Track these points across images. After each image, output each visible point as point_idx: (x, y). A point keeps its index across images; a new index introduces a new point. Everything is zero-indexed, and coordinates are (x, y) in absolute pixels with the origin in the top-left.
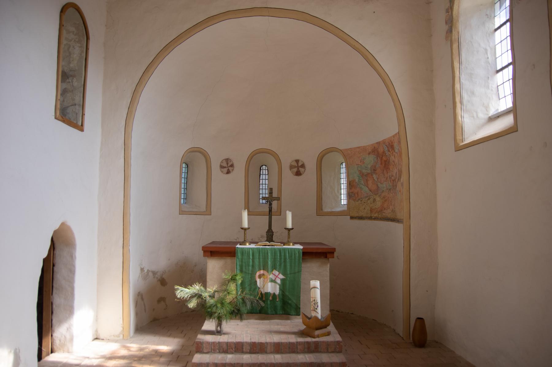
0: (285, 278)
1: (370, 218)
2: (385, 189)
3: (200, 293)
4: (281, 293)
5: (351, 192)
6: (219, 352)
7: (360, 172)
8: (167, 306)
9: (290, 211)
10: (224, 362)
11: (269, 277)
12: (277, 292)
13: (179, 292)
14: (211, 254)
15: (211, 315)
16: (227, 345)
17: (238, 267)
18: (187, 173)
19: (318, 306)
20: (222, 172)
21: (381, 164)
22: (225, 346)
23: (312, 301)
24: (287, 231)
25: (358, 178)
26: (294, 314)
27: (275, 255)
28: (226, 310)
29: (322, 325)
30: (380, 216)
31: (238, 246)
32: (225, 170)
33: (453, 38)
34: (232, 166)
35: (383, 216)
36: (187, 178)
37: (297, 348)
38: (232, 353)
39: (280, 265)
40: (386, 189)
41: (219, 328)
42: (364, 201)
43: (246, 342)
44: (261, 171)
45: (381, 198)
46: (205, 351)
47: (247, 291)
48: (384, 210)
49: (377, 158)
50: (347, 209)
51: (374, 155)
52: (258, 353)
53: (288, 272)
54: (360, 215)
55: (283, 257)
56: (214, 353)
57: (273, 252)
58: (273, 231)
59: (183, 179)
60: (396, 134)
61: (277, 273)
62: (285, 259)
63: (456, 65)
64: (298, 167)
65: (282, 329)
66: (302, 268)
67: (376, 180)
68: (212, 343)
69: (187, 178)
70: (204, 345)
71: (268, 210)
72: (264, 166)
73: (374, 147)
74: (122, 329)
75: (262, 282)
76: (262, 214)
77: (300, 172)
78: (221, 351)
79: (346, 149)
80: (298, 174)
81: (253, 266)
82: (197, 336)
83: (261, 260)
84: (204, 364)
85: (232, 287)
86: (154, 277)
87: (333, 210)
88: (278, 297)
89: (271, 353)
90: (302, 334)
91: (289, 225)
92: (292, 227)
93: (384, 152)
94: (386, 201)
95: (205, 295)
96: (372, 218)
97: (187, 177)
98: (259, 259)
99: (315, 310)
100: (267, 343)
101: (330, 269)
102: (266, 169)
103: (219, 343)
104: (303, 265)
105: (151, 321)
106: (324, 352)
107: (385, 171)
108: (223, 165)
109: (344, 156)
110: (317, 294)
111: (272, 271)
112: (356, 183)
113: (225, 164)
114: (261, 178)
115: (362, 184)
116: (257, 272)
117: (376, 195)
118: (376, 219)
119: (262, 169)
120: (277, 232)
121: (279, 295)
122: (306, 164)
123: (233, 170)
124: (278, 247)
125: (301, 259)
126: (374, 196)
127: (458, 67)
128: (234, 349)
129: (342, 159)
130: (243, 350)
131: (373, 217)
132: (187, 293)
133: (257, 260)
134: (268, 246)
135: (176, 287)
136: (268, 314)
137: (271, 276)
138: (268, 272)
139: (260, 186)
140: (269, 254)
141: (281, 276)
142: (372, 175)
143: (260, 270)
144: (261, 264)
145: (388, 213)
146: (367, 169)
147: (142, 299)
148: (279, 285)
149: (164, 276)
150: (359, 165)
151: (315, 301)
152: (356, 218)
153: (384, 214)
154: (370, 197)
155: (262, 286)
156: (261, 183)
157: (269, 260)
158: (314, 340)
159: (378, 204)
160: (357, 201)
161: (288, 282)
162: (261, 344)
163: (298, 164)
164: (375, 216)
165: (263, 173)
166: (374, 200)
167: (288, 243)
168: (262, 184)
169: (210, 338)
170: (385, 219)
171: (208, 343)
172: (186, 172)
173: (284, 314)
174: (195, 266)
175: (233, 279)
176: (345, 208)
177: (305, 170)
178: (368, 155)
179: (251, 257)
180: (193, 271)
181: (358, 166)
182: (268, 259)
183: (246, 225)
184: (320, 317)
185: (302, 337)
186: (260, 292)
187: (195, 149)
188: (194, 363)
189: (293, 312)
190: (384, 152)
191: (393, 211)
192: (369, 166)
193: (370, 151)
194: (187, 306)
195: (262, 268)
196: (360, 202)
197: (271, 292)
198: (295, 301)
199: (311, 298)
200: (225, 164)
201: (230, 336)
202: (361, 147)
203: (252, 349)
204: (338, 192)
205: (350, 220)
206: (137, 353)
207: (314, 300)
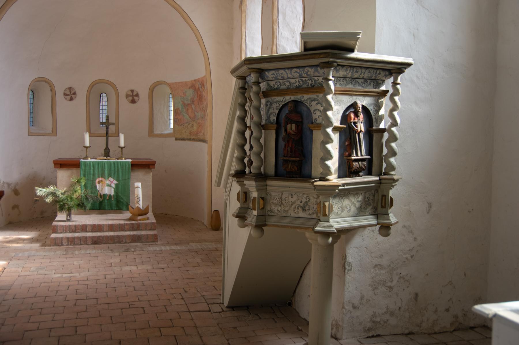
0: (118, 183)
1: (189, 140)
2: (199, 117)
3: (55, 192)
4: (115, 194)
6: (70, 232)
7: (183, 102)
8: (20, 212)
9: (122, 133)
11: (106, 183)
13: (38, 191)
14: (60, 166)
15: (62, 208)
16: (75, 227)
18: (33, 99)
19: (140, 200)
20: (66, 99)
21: (197, 97)
22: (73, 228)
23: (136, 196)
24: (120, 149)
26: (125, 209)
28: (74, 202)
29: (144, 213)
30: (196, 138)
31: (82, 160)
32: (69, 97)
33: (242, 9)
34: (75, 94)
36: (33, 104)
37: (125, 227)
38: (79, 232)
39: (114, 174)
43: (89, 225)
44: (101, 98)
46: (59, 232)
47: (89, 190)
48: (199, 133)
49: (195, 92)
50: (393, 105)
53: (121, 179)
55: (116, 168)
56: (66, 233)
57: (109, 164)
60: (205, 76)
61: (112, 179)
62: (118, 169)
63: (244, 30)
64: (133, 96)
66: (131, 176)
67: (194, 109)
68: (64, 226)
69: (33, 104)
70: (58, 227)
71: (105, 132)
72: (104, 95)
73: (193, 83)
75: (101, 186)
76: (100, 136)
77: (135, 100)
78: (71, 231)
79: (172, 83)
80: (133, 102)
81: (94, 175)
82: (52, 223)
83: (100, 170)
84: (59, 238)
86: (9, 188)
87: (162, 133)
88: (113, 198)
91: (122, 144)
92: (124, 145)
93: (199, 88)
94: (200, 126)
95: (58, 193)
97: (33, 103)
98: (98, 169)
99: (138, 203)
100: (104, 225)
101: (152, 176)
102: (106, 96)
105: (7, 224)
107: (200, 103)
108: (66, 92)
109: (171, 88)
110: (139, 192)
111: (108, 178)
113: (68, 92)
116: (96, 179)
117: (194, 121)
118: (193, 140)
119: (101, 96)
120: (116, 150)
121: (113, 195)
122: (140, 93)
123: (75, 97)
124: (113, 160)
125: (130, 169)
126: (193, 122)
127: (245, 31)
128: (80, 230)
129: (169, 91)
130: (87, 230)
131: (192, 139)
132: (44, 192)
133: (97, 170)
134: (105, 160)
135: (36, 188)
136: (105, 210)
138: (105, 179)
139: (100, 111)
140: (106, 166)
141: (115, 182)
142: (191, 105)
143: (99, 177)
144: (100, 173)
145: (201, 136)
148: (114, 189)
149: (17, 188)
150: (182, 96)
151: (138, 197)
155: (101, 190)
157: (106, 170)
158: (136, 222)
159: (195, 128)
160: (180, 126)
161: (120, 186)
162: (100, 226)
164: (193, 137)
165: (102, 100)
166: (193, 126)
167: (121, 158)
168: (102, 110)
170: (200, 140)
171: (61, 226)
172: (32, 98)
173: (118, 210)
174: (44, 179)
175: (79, 182)
176: (172, 131)
177: (139, 98)
180: (42, 183)
182: (105, 169)
183: (87, 144)
184: (141, 208)
186: (100, 194)
187: (41, 79)
190: (199, 88)
191: (204, 134)
192: (189, 98)
194: (45, 201)
195: (100, 176)
197: (108, 194)
198: (126, 200)
199: (135, 195)
200: (68, 92)
201: (77, 222)
203: (93, 229)
204: (167, 117)
207: (137, 196)
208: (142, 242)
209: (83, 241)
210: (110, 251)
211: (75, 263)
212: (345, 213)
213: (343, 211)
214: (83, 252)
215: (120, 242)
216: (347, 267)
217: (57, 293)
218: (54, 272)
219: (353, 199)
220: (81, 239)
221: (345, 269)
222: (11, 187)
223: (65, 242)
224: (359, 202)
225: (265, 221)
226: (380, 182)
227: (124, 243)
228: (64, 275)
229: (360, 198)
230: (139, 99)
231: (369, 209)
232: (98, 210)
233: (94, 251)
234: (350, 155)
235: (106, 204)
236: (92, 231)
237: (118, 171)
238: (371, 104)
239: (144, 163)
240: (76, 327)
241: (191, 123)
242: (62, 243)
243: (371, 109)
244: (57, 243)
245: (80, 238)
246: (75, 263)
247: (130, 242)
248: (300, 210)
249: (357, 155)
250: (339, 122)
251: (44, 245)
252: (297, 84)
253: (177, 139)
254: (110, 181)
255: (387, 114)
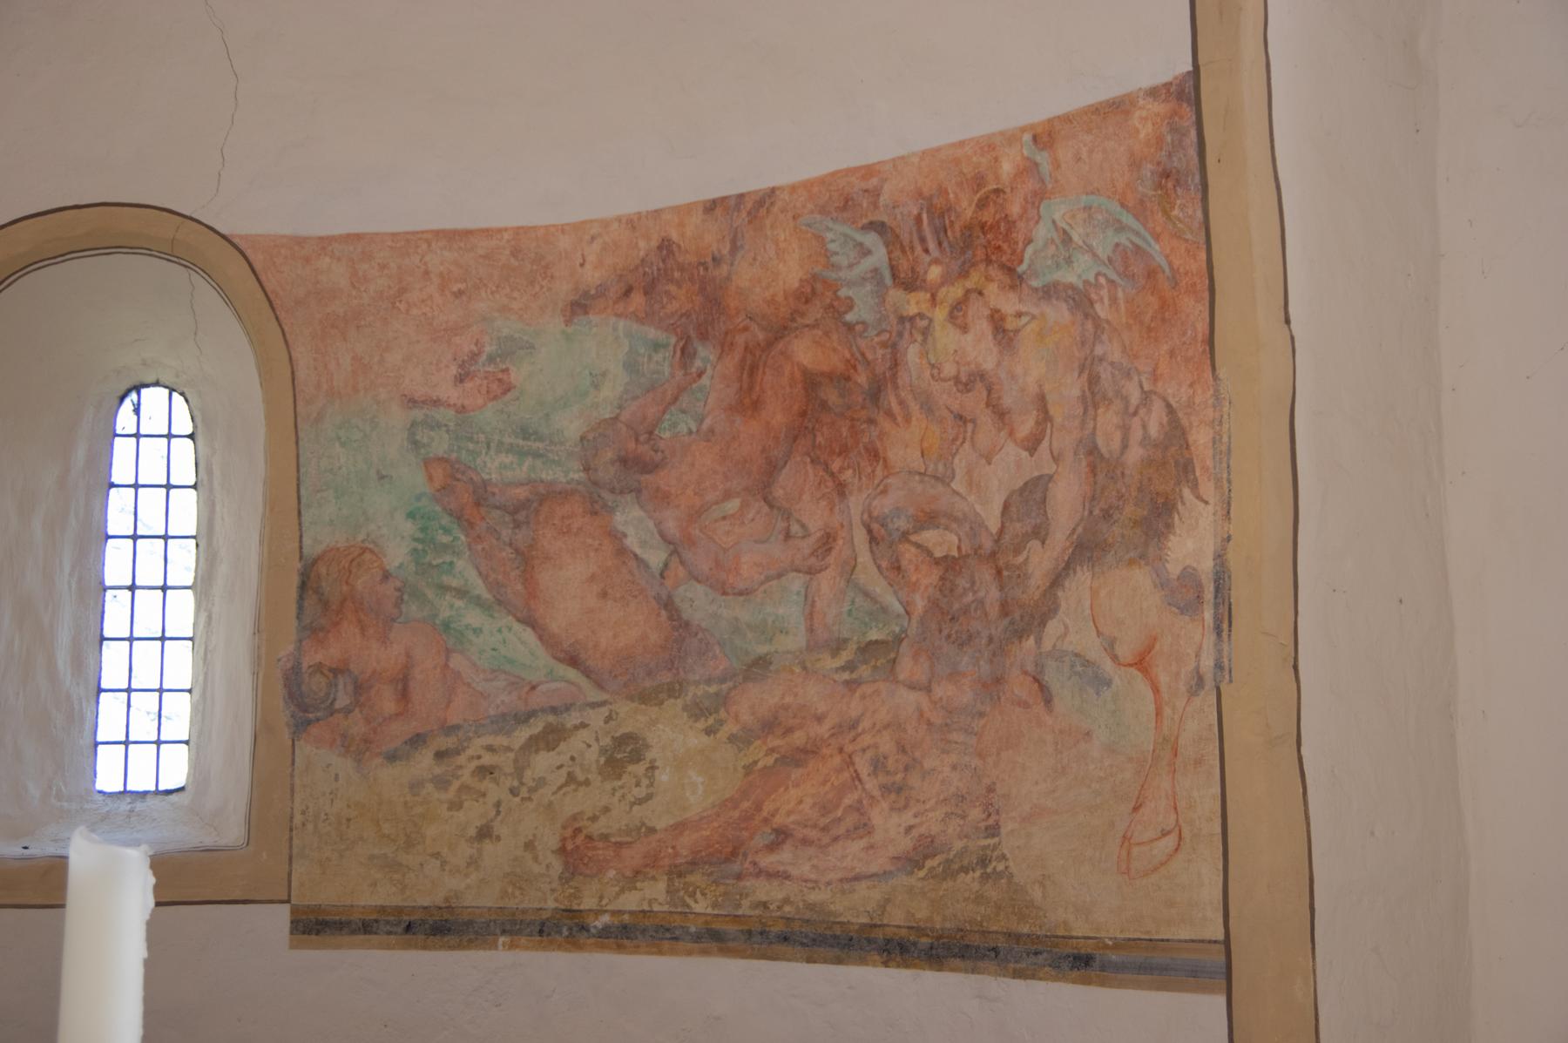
5: (318, 668)
25: (409, 528)
30: (700, 906)
35: (745, 910)
40: (811, 647)
42: (488, 759)
45: (730, 728)
51: (644, 318)
54: (425, 901)
79: (300, 241)
96: (584, 928)
112: (386, 576)
115: (461, 593)
146: (537, 455)
150: (436, 403)
152: (366, 928)
153: (764, 890)
154: (572, 719)
160: (392, 757)
164: (631, 901)
178: (568, 322)
181: (418, 414)
192: (571, 426)
193: (592, 276)
196: (424, 763)
202: (487, 233)
205: (292, 947)
241: (596, 718)
255: (1214, 734)
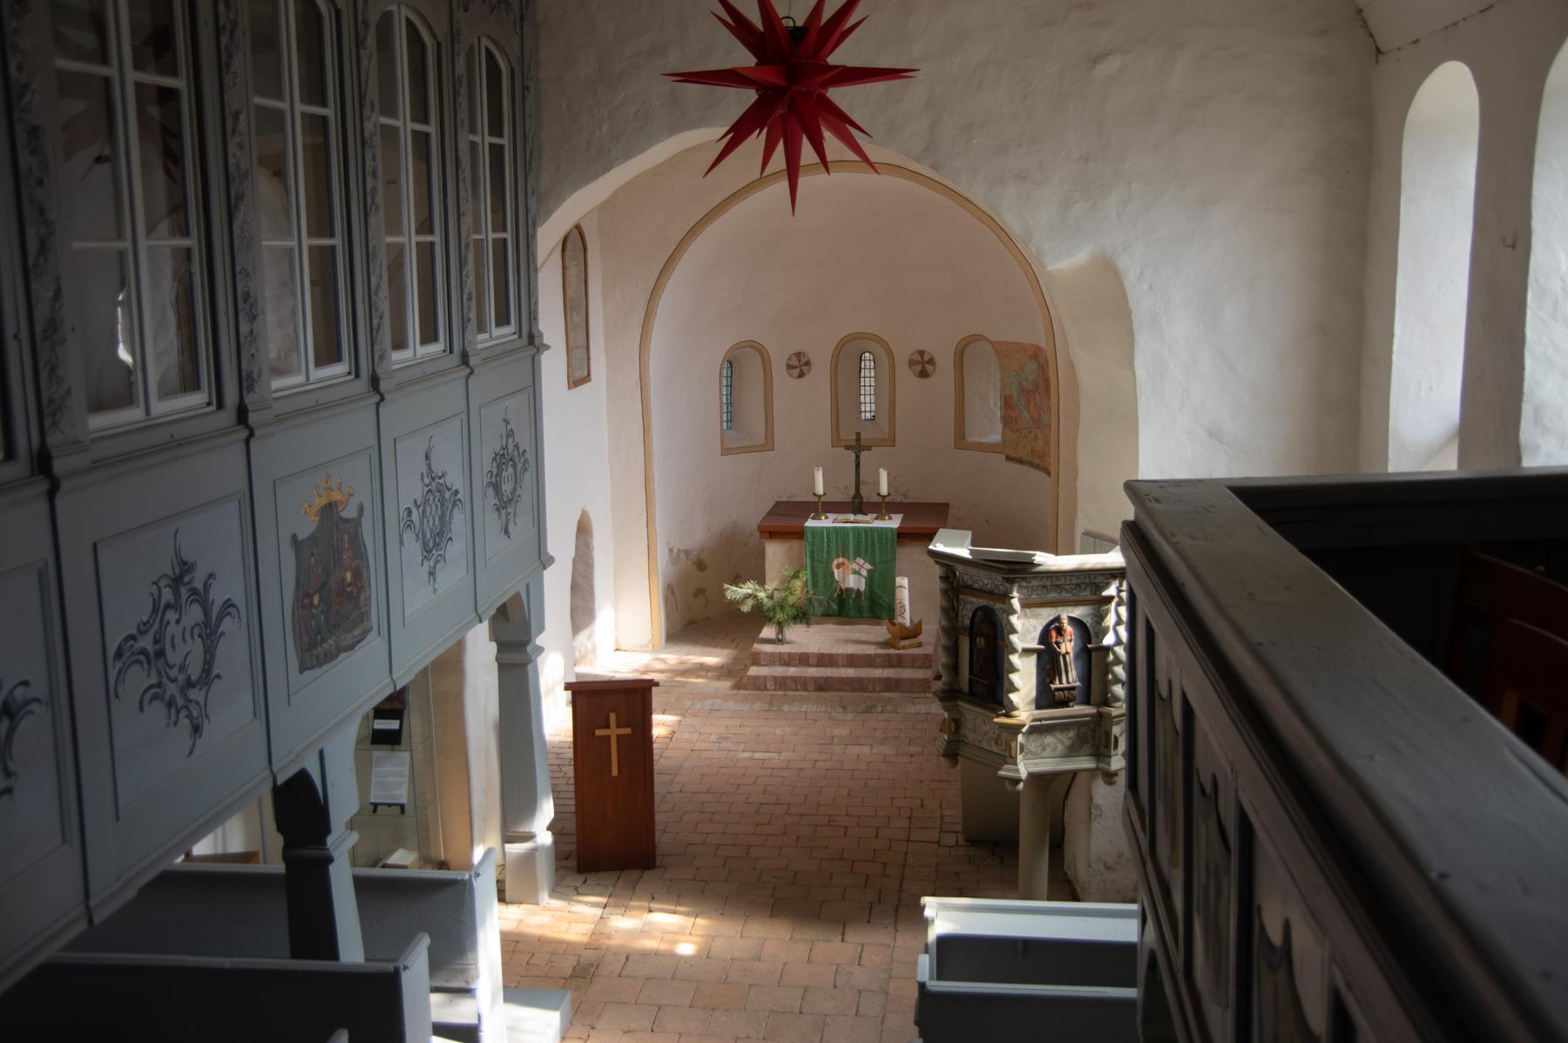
6: (781, 665)
7: (1019, 383)
9: (885, 468)
10: (784, 675)
12: (863, 587)
17: (808, 553)
20: (791, 375)
22: (786, 658)
27: (858, 542)
29: (914, 632)
32: (796, 372)
34: (808, 363)
41: (780, 636)
46: (763, 663)
52: (827, 666)
53: (878, 561)
58: (862, 495)
59: (724, 388)
61: (862, 561)
64: (923, 363)
65: (864, 637)
72: (867, 354)
74: (651, 636)
78: (783, 663)
80: (924, 374)
81: (829, 552)
82: (753, 645)
85: (798, 584)
86: (687, 559)
89: (843, 666)
90: (886, 644)
95: (762, 595)
98: (837, 542)
100: (838, 654)
103: (780, 653)
104: (898, 550)
105: (686, 625)
106: (909, 667)
108: (790, 363)
113: (795, 362)
114: (862, 375)
116: (833, 560)
123: (809, 370)
133: (834, 543)
135: (726, 586)
136: (850, 617)
137: (854, 566)
141: (868, 566)
143: (838, 557)
144: (840, 550)
147: (673, 593)
156: (862, 384)
157: (851, 543)
158: (897, 652)
161: (877, 575)
162: (831, 656)
163: (922, 357)
169: (769, 648)
171: (767, 654)
172: (729, 374)
179: (826, 540)
185: (884, 648)
188: (750, 676)
189: (884, 615)
195: (841, 554)
200: (795, 362)
201: (795, 645)
206: (677, 667)
208: (902, 692)
209: (800, 683)
210: (841, 710)
211: (778, 731)
212: (1048, 752)
213: (1044, 749)
214: (795, 709)
215: (863, 690)
216: (1094, 811)
217: (738, 788)
218: (742, 746)
219: (1059, 736)
220: (796, 681)
221: (1090, 813)
222: (691, 557)
223: (770, 685)
224: (1070, 738)
225: (958, 749)
226: (1100, 715)
227: (870, 692)
228: (757, 755)
229: (1071, 734)
230: (934, 370)
231: (1087, 749)
232: (835, 616)
233: (814, 708)
234: (1052, 682)
235: (851, 607)
236: (818, 665)
237: (873, 545)
238: (1088, 616)
239: (921, 532)
240: (750, 846)
242: (765, 685)
243: (1088, 621)
244: (758, 684)
245: (795, 679)
246: (778, 731)
247: (881, 691)
248: (993, 742)
249: (1061, 683)
250: (1036, 641)
251: (737, 687)
252: (989, 586)
253: (1008, 458)
254: (859, 565)
